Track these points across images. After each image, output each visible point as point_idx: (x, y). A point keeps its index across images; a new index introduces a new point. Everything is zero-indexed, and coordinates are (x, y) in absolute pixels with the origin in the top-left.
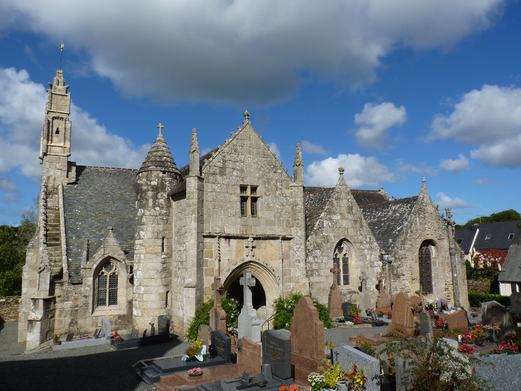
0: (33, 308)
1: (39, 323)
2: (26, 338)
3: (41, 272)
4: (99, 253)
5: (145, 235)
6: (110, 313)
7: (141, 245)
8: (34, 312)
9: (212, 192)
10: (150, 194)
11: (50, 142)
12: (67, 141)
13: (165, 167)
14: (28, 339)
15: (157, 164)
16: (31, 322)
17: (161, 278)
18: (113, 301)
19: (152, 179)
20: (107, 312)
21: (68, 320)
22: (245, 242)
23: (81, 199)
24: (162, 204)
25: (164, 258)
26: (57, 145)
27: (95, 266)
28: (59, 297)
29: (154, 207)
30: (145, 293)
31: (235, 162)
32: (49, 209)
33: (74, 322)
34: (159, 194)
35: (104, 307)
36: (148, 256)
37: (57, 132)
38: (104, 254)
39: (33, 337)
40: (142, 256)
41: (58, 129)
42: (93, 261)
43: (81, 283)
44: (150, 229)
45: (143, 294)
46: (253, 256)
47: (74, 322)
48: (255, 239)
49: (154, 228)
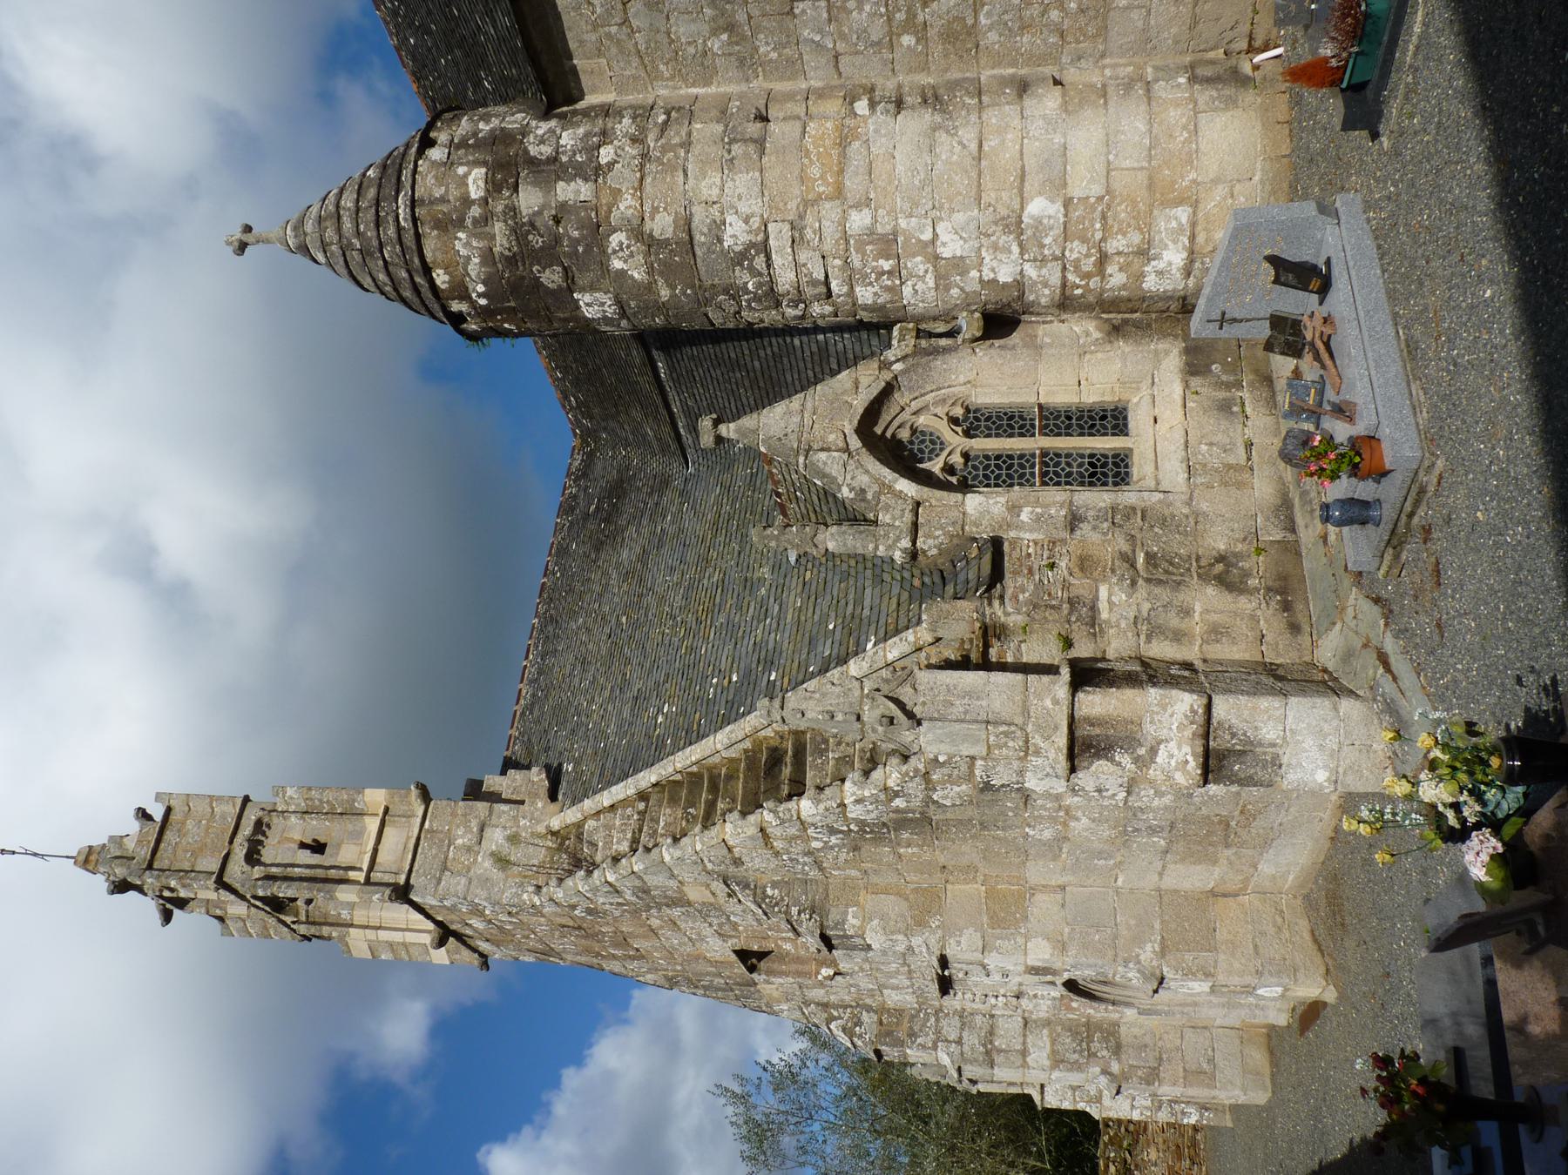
0: (1126, 760)
1: (1224, 708)
2: (1316, 793)
3: (910, 715)
4: (834, 470)
5: (744, 208)
6: (1171, 415)
8: (1153, 751)
11: (352, 875)
14: (1321, 776)
16: (1213, 765)
17: (981, 107)
18: (1112, 419)
19: (454, 193)
20: (1168, 423)
21: (1205, 601)
24: (587, 135)
25: (873, 105)
28: (1068, 643)
29: (594, 172)
30: (1058, 185)
33: (1220, 567)
34: (533, 151)
35: (1136, 459)
36: (854, 184)
37: (318, 848)
38: (847, 450)
39: (1309, 743)
40: (859, 221)
41: (303, 846)
42: (877, 495)
43: (996, 544)
44: (708, 186)
45: (1068, 203)
47: (1220, 567)
49: (705, 163)
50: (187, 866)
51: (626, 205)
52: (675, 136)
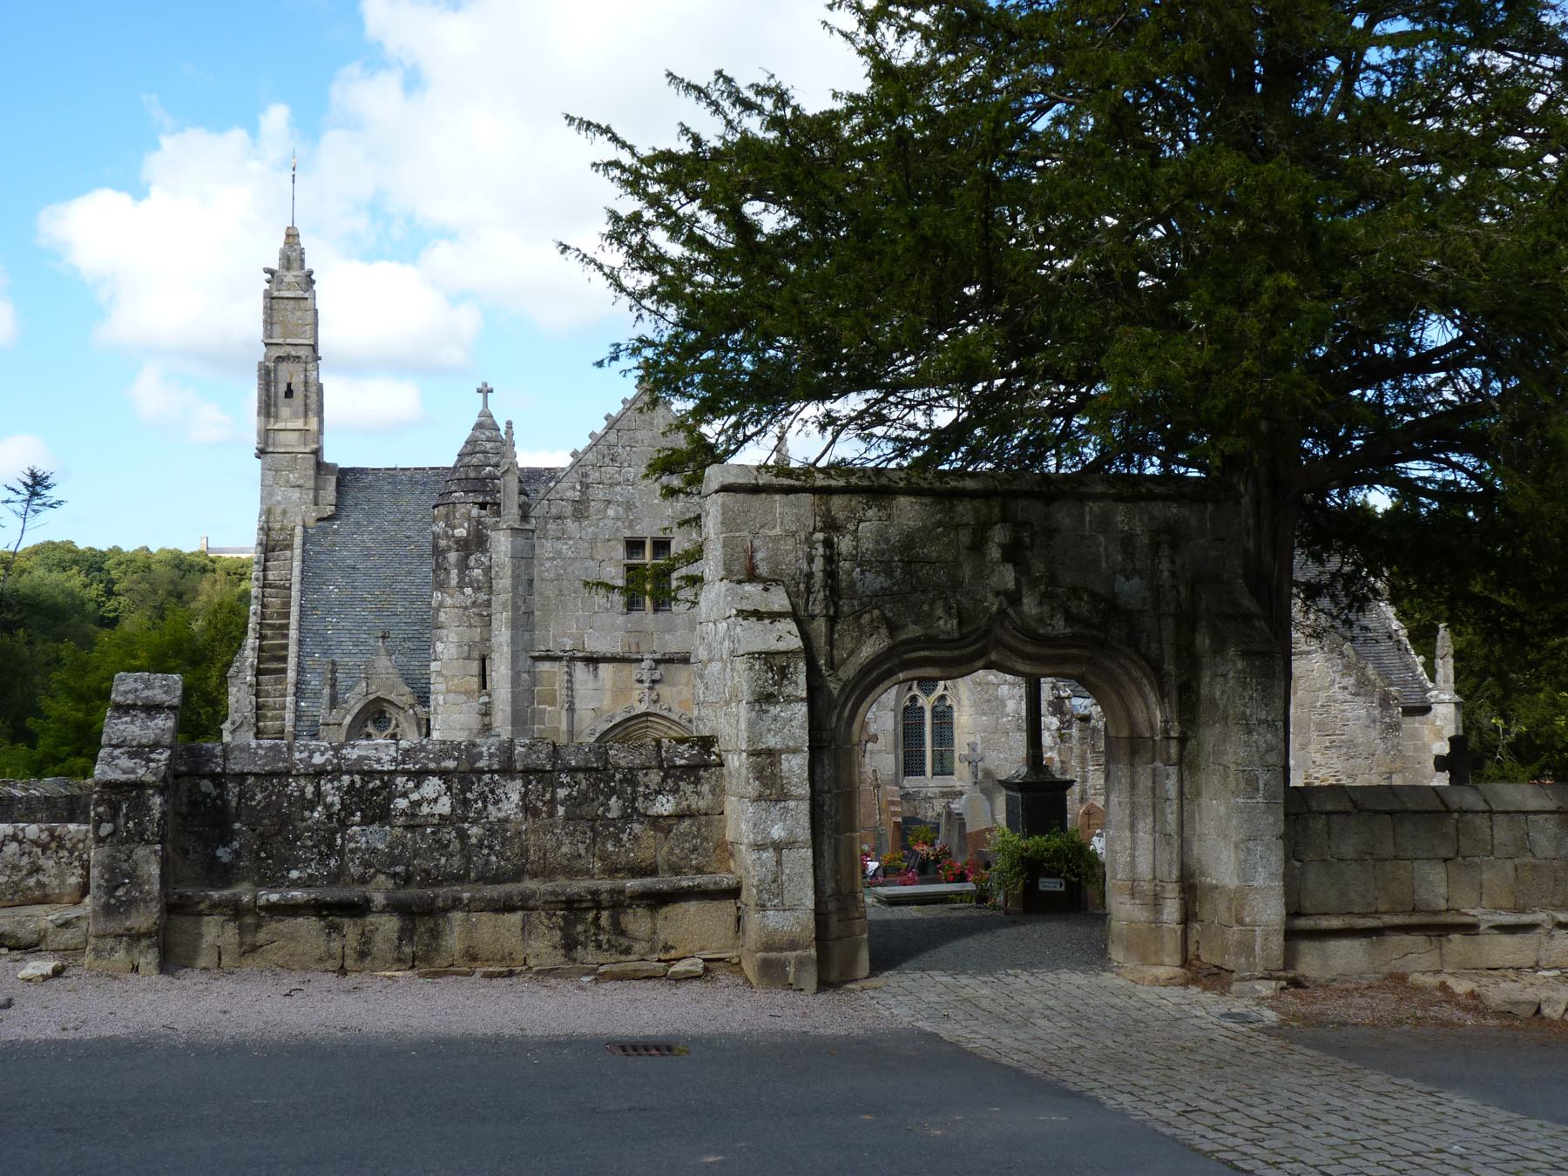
7: (439, 673)
9: (554, 558)
10: (453, 557)
12: (310, 414)
13: (484, 492)
15: (470, 486)
19: (457, 522)
22: (634, 671)
23: (343, 560)
26: (290, 426)
27: (349, 719)
31: (611, 485)
32: (270, 586)
37: (289, 393)
40: (441, 698)
41: (289, 385)
44: (453, 637)
46: (655, 702)
48: (657, 662)
49: (460, 634)
50: (275, 319)
51: (449, 601)
52: (475, 621)
